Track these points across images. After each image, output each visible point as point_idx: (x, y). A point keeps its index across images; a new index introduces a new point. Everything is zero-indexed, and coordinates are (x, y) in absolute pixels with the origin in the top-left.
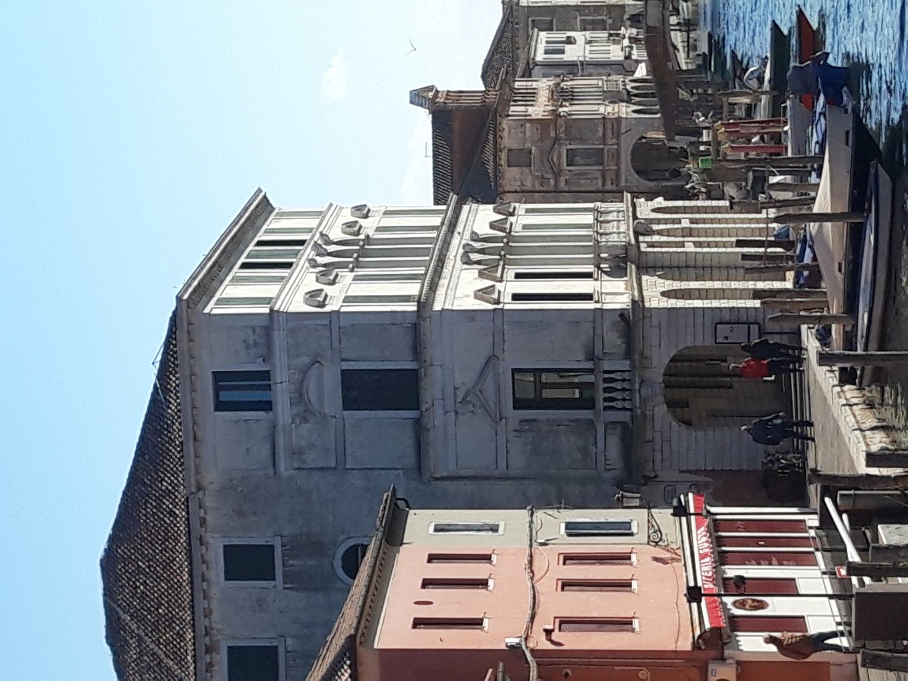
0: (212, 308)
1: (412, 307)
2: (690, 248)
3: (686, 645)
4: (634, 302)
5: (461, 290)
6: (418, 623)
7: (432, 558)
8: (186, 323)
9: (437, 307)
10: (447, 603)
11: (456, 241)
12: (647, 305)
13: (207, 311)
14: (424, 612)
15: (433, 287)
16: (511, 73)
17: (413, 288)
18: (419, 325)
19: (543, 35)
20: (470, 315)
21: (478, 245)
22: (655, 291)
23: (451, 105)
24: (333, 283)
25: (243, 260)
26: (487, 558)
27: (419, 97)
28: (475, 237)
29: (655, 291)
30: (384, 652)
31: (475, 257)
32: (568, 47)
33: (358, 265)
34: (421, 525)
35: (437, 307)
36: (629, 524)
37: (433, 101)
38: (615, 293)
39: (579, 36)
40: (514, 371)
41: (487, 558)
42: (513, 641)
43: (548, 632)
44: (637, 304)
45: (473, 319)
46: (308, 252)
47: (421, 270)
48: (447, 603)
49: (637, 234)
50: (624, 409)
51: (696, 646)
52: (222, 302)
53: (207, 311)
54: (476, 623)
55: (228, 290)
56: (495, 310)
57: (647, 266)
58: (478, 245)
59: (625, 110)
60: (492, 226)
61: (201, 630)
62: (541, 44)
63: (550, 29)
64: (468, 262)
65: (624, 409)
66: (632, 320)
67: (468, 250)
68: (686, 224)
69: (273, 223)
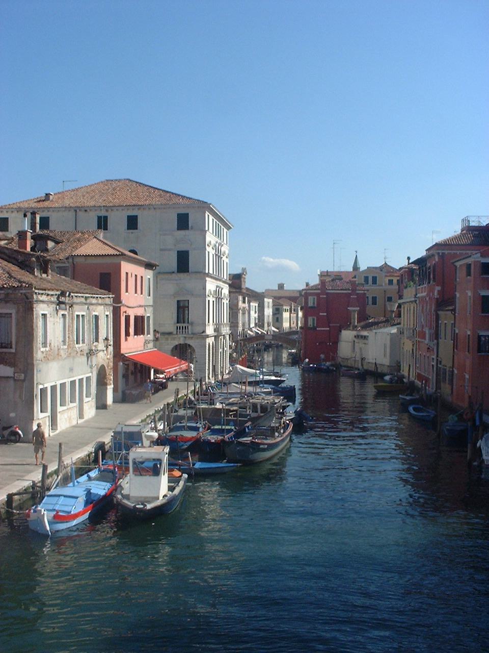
0: (207, 213)
1: (207, 272)
2: (220, 351)
3: (122, 352)
4: (208, 335)
5: (211, 285)
6: (127, 273)
7: (142, 277)
8: (204, 206)
9: (207, 279)
10: (131, 281)
11: (221, 283)
12: (207, 339)
13: (207, 212)
14: (129, 275)
15: (212, 277)
16: (249, 296)
17: (211, 272)
18: (203, 275)
19: (257, 305)
20: (205, 288)
21: (220, 290)
22: (210, 341)
23: (242, 279)
24: (213, 248)
25: (220, 224)
26: (142, 293)
27: (244, 270)
28: (222, 289)
29: (210, 341)
30: (120, 263)
31: (218, 289)
32: (254, 312)
33: (216, 255)
34: (149, 274)
35: (207, 279)
36: (149, 334)
37: (243, 274)
38: (210, 330)
39: (256, 315)
40: (188, 301)
41: (142, 293)
42: (123, 302)
43: (126, 312)
44: (208, 336)
45: (203, 289)
46: (219, 241)
47: (215, 273)
48: (131, 281)
49: (224, 335)
50: (177, 332)
51: (123, 355)
52: (208, 215)
53: (207, 212)
54: (127, 291)
55: (211, 218)
56: (206, 295)
57: (216, 337)
58: (220, 290)
59: (240, 329)
60: (225, 294)
61: (113, 208)
62: (254, 305)
63: (258, 306)
64: (217, 287)
65: (177, 332)
66: (203, 336)
67: (219, 287)
68: (225, 349)
69: (225, 230)
